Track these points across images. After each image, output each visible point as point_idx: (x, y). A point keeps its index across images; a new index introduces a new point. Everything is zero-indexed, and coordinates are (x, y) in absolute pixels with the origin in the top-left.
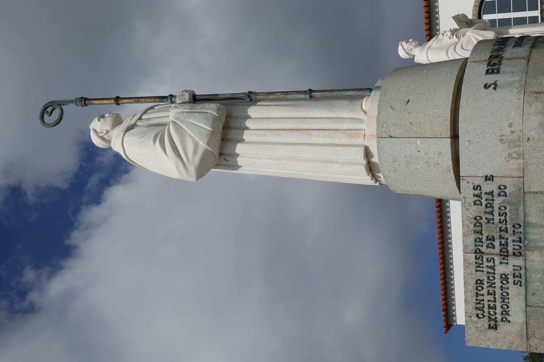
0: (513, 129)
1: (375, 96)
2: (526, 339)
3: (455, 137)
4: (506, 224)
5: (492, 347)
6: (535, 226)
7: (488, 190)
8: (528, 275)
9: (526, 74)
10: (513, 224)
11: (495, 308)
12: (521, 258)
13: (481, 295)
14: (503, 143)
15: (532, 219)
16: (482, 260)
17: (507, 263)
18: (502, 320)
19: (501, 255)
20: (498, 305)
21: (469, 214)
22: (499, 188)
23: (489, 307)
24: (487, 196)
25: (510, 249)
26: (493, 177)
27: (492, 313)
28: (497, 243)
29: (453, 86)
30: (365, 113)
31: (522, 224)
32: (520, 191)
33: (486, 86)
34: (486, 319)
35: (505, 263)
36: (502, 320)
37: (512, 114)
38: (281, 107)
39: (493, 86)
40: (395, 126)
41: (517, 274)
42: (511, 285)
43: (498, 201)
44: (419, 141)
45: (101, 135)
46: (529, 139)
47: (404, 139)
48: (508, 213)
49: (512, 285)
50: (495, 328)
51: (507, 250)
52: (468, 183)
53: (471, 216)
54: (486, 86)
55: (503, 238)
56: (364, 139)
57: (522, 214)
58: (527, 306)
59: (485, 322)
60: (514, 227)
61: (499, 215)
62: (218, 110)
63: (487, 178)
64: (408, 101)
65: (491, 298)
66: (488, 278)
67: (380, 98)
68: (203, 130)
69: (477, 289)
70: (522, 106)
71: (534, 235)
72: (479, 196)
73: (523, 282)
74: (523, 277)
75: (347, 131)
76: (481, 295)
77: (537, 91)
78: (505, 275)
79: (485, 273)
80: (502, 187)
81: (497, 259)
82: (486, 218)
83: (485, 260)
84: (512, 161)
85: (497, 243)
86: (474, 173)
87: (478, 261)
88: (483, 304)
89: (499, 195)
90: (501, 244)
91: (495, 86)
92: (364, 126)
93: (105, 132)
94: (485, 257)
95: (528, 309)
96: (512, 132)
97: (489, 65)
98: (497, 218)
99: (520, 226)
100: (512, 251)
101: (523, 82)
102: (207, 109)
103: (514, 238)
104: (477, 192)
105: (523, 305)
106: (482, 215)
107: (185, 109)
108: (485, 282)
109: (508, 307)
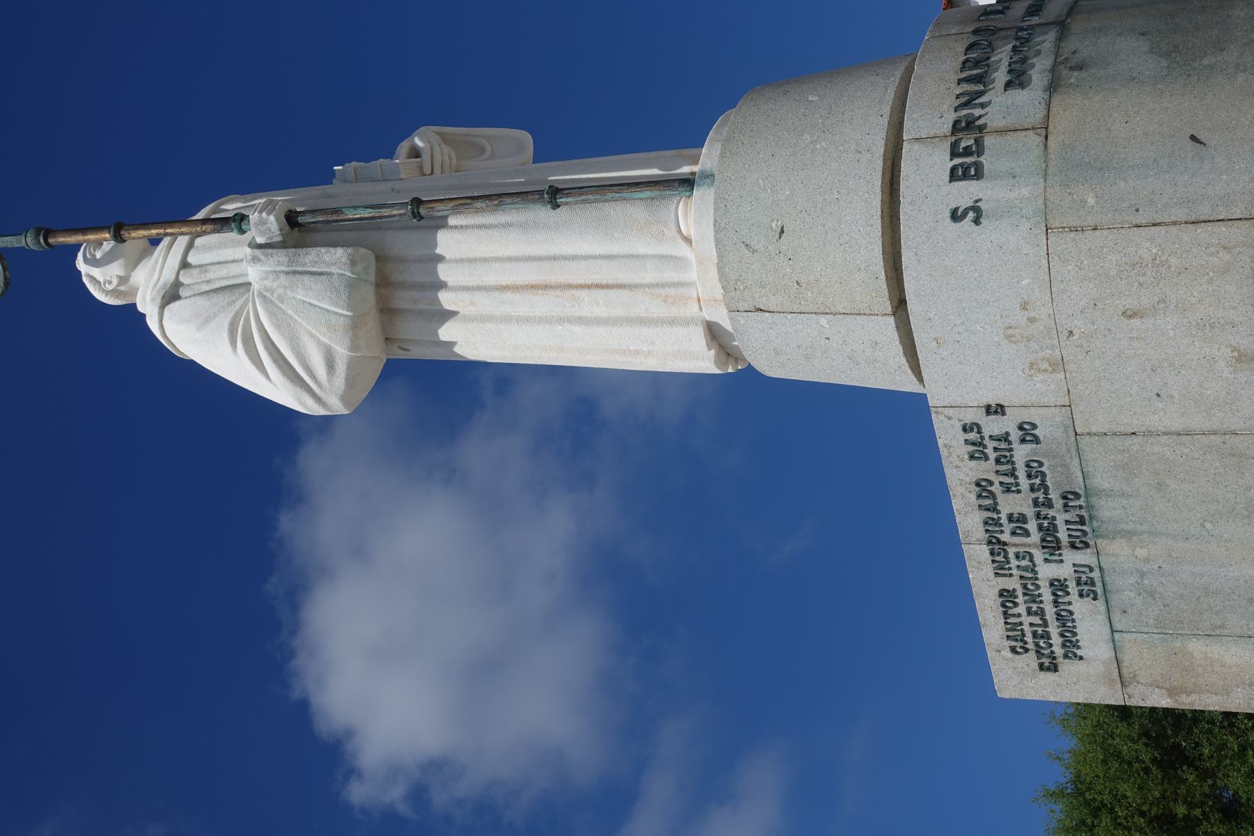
0: (1032, 315)
1: (703, 196)
2: (1119, 685)
3: (900, 304)
4: (1046, 493)
5: (1052, 699)
6: (1110, 494)
7: (997, 431)
8: (1107, 579)
9: (1045, 180)
10: (1060, 492)
11: (1046, 636)
12: (1089, 551)
13: (1014, 615)
14: (1014, 343)
15: (1101, 481)
16: (1006, 557)
17: (1061, 561)
18: (1066, 656)
19: (1043, 547)
20: (1054, 630)
21: (962, 476)
22: (1021, 428)
23: (1035, 634)
24: (995, 444)
25: (1063, 535)
26: (1002, 407)
27: (1041, 644)
28: (1032, 526)
29: (878, 190)
30: (688, 240)
31: (1081, 492)
32: (1066, 431)
33: (956, 216)
34: (1032, 654)
35: (1055, 561)
36: (1066, 656)
37: (1026, 282)
38: (495, 233)
39: (971, 215)
40: (763, 287)
41: (1084, 578)
42: (1074, 596)
43: (1021, 453)
44: (823, 320)
45: (109, 287)
46: (1071, 332)
47: (789, 316)
48: (1047, 472)
49: (1076, 596)
50: (1054, 668)
51: (1057, 538)
52: (950, 418)
53: (968, 479)
54: (956, 216)
55: (1045, 518)
56: (701, 309)
57: (1079, 474)
58: (1113, 631)
59: (1031, 659)
60: (1064, 498)
61: (1029, 476)
62: (353, 263)
63: (989, 410)
64: (782, 232)
65: (1037, 620)
66: (1025, 586)
67: (715, 221)
68: (333, 318)
69: (1003, 605)
70: (1044, 262)
71: (1107, 510)
72: (980, 444)
73: (1099, 591)
74: (1099, 584)
75: (657, 291)
76: (1014, 615)
77: (1075, 224)
78: (1059, 581)
79: (1016, 578)
80: (1026, 427)
81: (1039, 556)
82: (1001, 483)
83: (1011, 555)
84: (1040, 377)
85: (1032, 526)
86: (959, 401)
87: (997, 558)
88: (1022, 630)
89: (1023, 441)
90: (1040, 528)
91: (976, 213)
92: (693, 276)
93: (115, 282)
94: (1011, 551)
95: (1117, 636)
96: (1032, 320)
97: (954, 154)
98: (1024, 483)
99: (1077, 496)
100: (1067, 539)
101: (1041, 201)
102: (329, 265)
103: (1068, 516)
104: (973, 436)
105: (1109, 630)
106: (992, 477)
107: (279, 264)
108: (1019, 592)
109: (1075, 634)
